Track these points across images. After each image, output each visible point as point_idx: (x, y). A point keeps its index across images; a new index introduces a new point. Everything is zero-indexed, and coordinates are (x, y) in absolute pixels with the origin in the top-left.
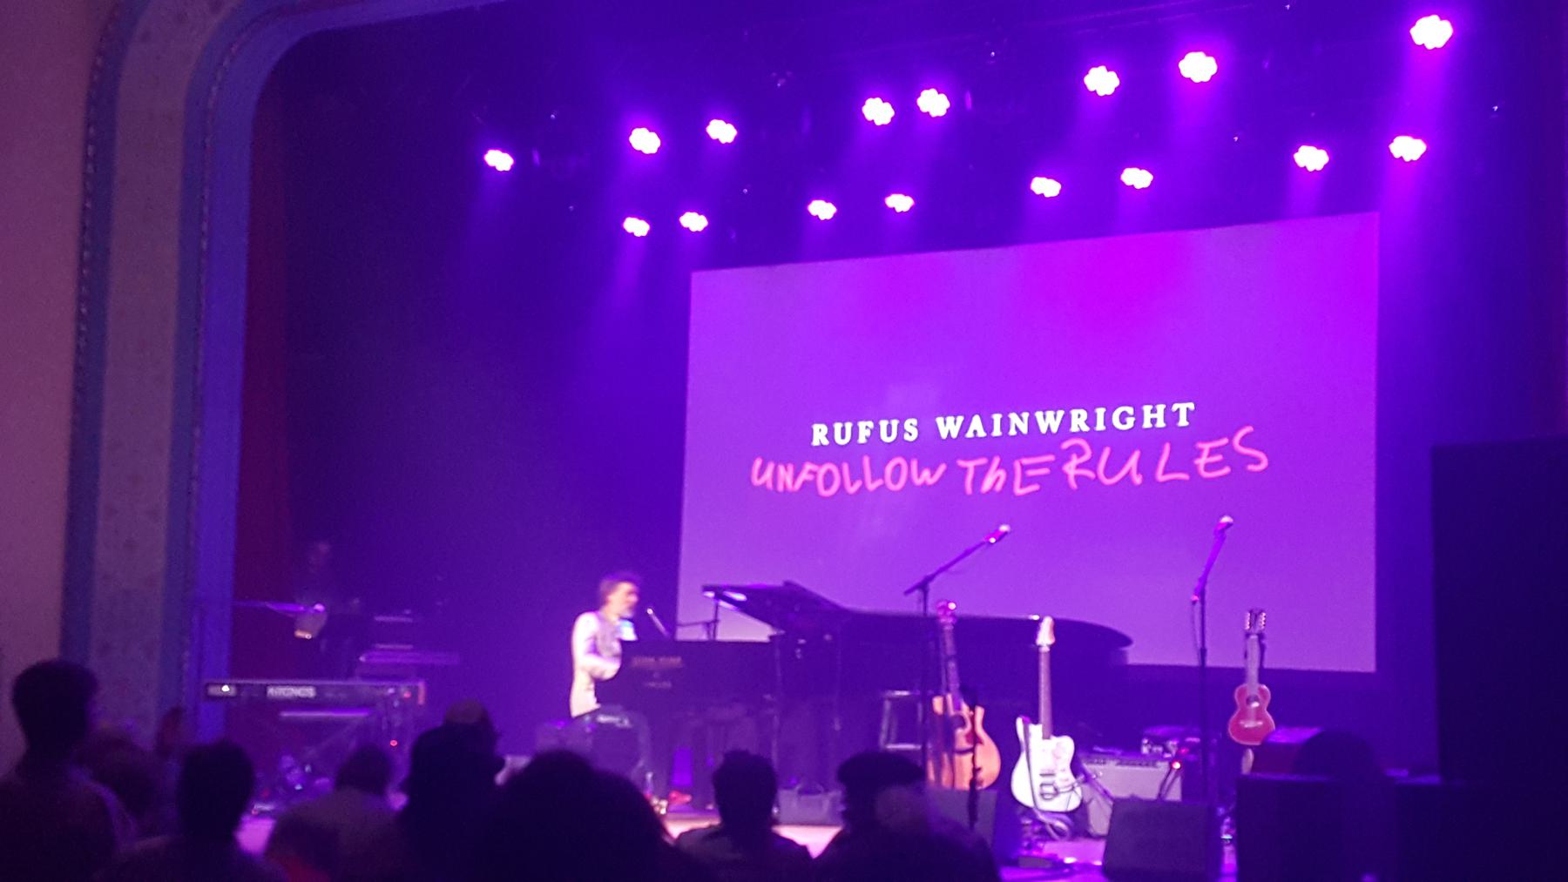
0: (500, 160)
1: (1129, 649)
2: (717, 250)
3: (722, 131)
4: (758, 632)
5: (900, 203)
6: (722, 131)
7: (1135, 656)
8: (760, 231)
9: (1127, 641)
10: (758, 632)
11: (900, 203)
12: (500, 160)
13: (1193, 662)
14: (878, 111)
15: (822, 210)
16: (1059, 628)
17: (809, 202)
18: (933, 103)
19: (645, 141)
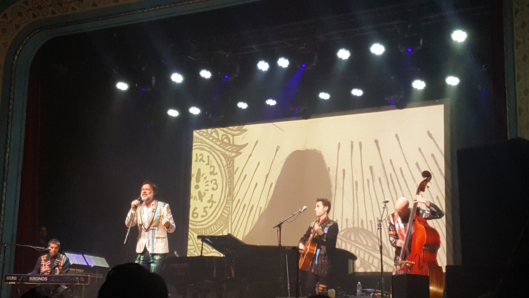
0: (122, 86)
1: (357, 263)
2: (205, 122)
3: (206, 74)
4: (215, 253)
5: (271, 102)
6: (206, 74)
7: (359, 267)
8: (221, 116)
9: (354, 258)
10: (215, 253)
11: (271, 102)
12: (122, 86)
13: (277, 244)
14: (263, 66)
15: (242, 105)
16: (355, 293)
17: (237, 103)
18: (283, 63)
19: (177, 78)
